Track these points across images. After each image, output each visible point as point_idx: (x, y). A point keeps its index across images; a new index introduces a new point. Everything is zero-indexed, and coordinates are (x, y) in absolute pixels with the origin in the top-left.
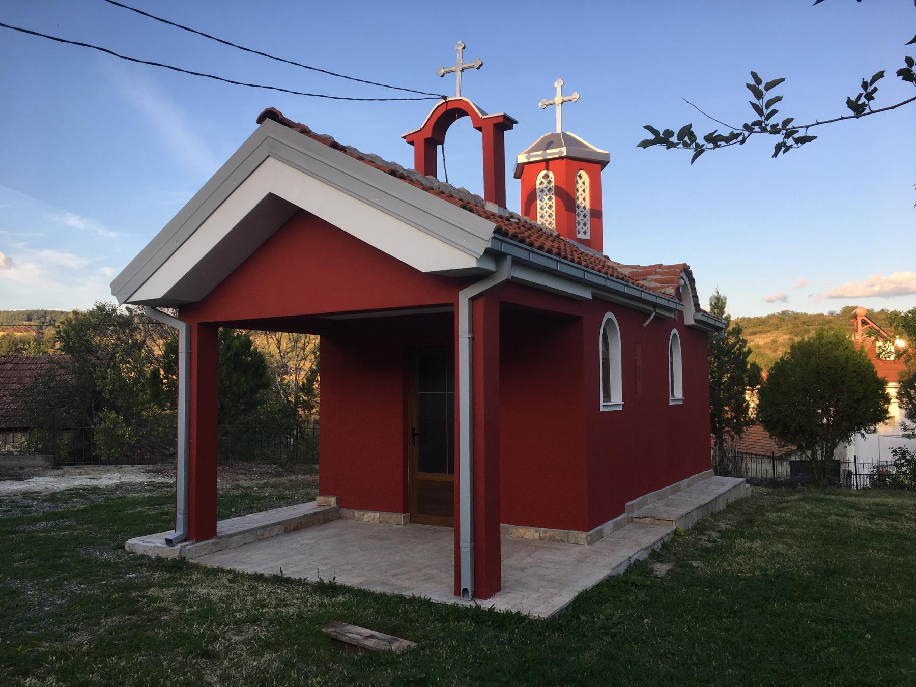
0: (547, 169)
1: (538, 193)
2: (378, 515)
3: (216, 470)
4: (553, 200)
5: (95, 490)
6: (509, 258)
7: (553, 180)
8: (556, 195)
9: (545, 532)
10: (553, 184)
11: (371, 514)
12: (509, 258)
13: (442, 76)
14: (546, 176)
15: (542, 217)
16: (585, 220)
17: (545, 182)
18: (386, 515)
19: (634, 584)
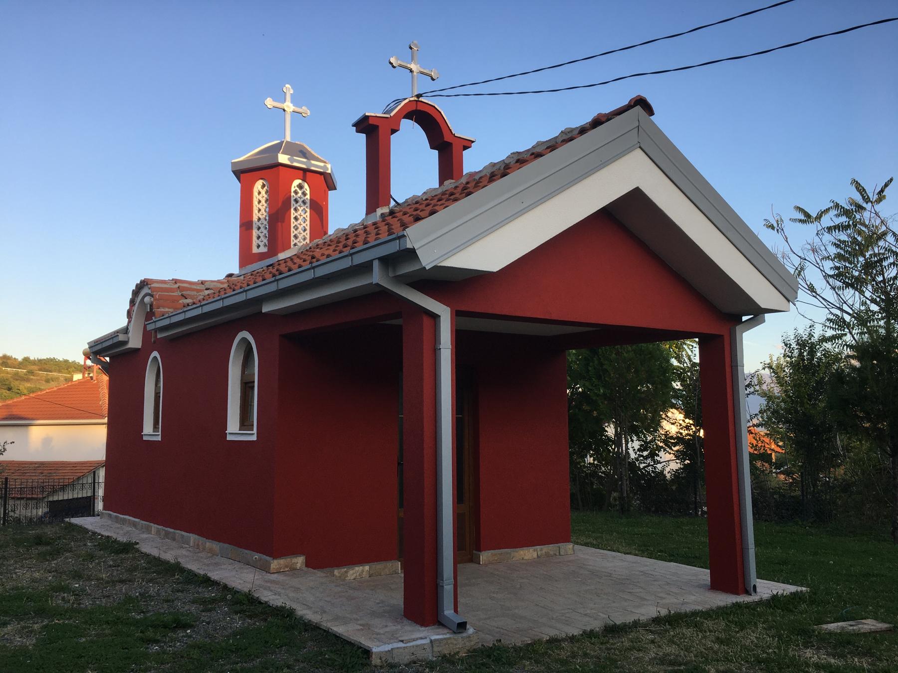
0: (304, 180)
1: (293, 202)
2: (367, 568)
3: (294, 553)
4: (308, 214)
5: (858, 635)
6: (376, 264)
7: (308, 192)
8: (310, 209)
9: (541, 550)
10: (308, 197)
11: (358, 569)
12: (376, 264)
13: (411, 48)
14: (300, 187)
15: (305, 230)
16: (296, 232)
17: (300, 192)
18: (378, 566)
19: (122, 581)
